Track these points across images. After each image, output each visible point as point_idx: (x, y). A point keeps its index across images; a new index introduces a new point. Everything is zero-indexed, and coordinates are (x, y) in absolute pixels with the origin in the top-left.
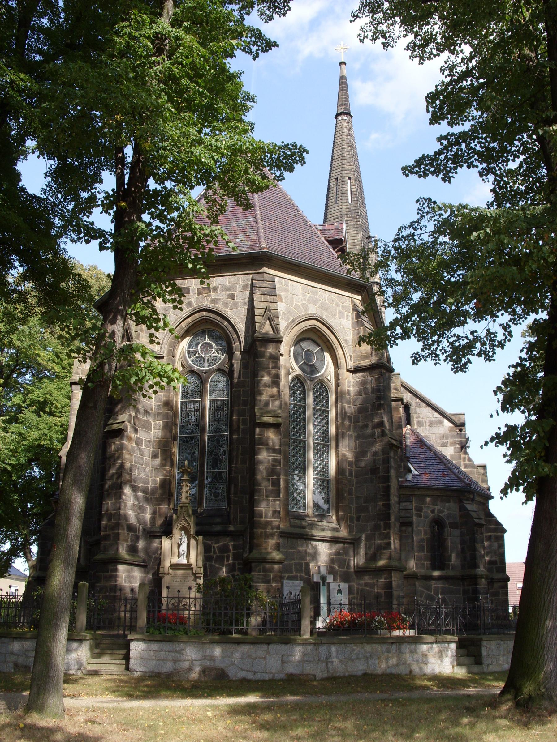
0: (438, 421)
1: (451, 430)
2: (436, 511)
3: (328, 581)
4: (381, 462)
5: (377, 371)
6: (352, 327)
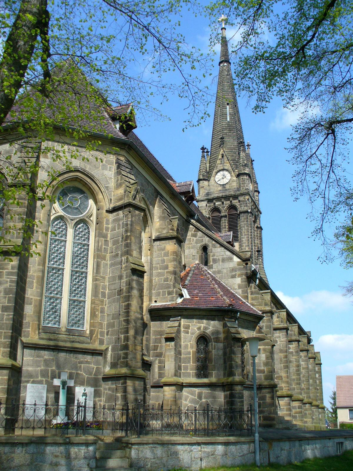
0: (229, 257)
1: (239, 264)
2: (202, 328)
3: (68, 385)
4: (125, 285)
5: (127, 209)
6: (114, 177)
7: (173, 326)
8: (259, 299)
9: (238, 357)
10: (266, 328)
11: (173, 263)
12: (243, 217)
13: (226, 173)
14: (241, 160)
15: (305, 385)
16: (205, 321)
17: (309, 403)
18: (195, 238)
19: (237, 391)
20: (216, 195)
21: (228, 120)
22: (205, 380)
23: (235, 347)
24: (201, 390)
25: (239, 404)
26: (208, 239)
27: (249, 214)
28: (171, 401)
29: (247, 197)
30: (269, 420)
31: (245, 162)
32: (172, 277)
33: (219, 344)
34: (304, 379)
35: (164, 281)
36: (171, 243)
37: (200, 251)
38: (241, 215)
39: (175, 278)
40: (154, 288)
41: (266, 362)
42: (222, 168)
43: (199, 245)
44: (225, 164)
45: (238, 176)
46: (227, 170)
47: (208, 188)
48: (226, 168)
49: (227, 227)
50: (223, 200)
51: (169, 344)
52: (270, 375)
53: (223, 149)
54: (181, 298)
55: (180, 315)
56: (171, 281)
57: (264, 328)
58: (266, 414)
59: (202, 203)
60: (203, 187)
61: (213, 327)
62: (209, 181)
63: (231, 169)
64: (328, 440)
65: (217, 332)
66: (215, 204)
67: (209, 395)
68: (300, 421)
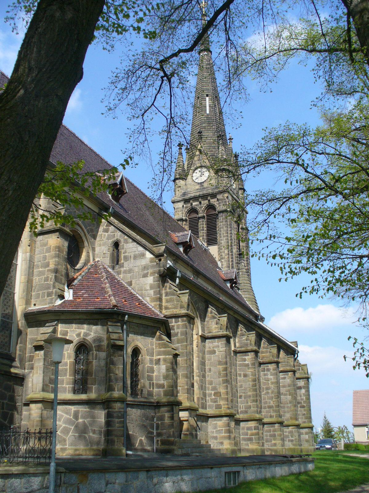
1: (151, 261)
2: (82, 335)
7: (46, 332)
8: (174, 300)
9: (118, 368)
10: (181, 335)
11: (54, 260)
12: (221, 217)
14: (220, 154)
15: (273, 402)
16: (85, 326)
17: (278, 423)
18: (106, 234)
19: (115, 409)
20: (193, 195)
21: (208, 112)
22: (83, 397)
23: (115, 357)
24: (77, 408)
25: (117, 425)
26: (120, 233)
28: (37, 421)
30: (168, 445)
31: (224, 157)
32: (52, 276)
33: (101, 353)
34: (273, 395)
35: (45, 281)
36: (53, 237)
37: (111, 248)
39: (56, 277)
40: (34, 290)
41: (166, 374)
42: (199, 165)
43: (110, 241)
45: (217, 172)
46: (205, 167)
47: (185, 187)
49: (205, 229)
50: (200, 200)
51: (39, 354)
52: (173, 390)
53: (201, 144)
54: (61, 300)
55: (58, 320)
56: (51, 281)
57: (179, 334)
58: (164, 437)
59: (179, 204)
61: (95, 333)
62: (186, 180)
64: (209, 470)
65: (98, 340)
66: (192, 204)
67: (87, 414)
68: (256, 444)
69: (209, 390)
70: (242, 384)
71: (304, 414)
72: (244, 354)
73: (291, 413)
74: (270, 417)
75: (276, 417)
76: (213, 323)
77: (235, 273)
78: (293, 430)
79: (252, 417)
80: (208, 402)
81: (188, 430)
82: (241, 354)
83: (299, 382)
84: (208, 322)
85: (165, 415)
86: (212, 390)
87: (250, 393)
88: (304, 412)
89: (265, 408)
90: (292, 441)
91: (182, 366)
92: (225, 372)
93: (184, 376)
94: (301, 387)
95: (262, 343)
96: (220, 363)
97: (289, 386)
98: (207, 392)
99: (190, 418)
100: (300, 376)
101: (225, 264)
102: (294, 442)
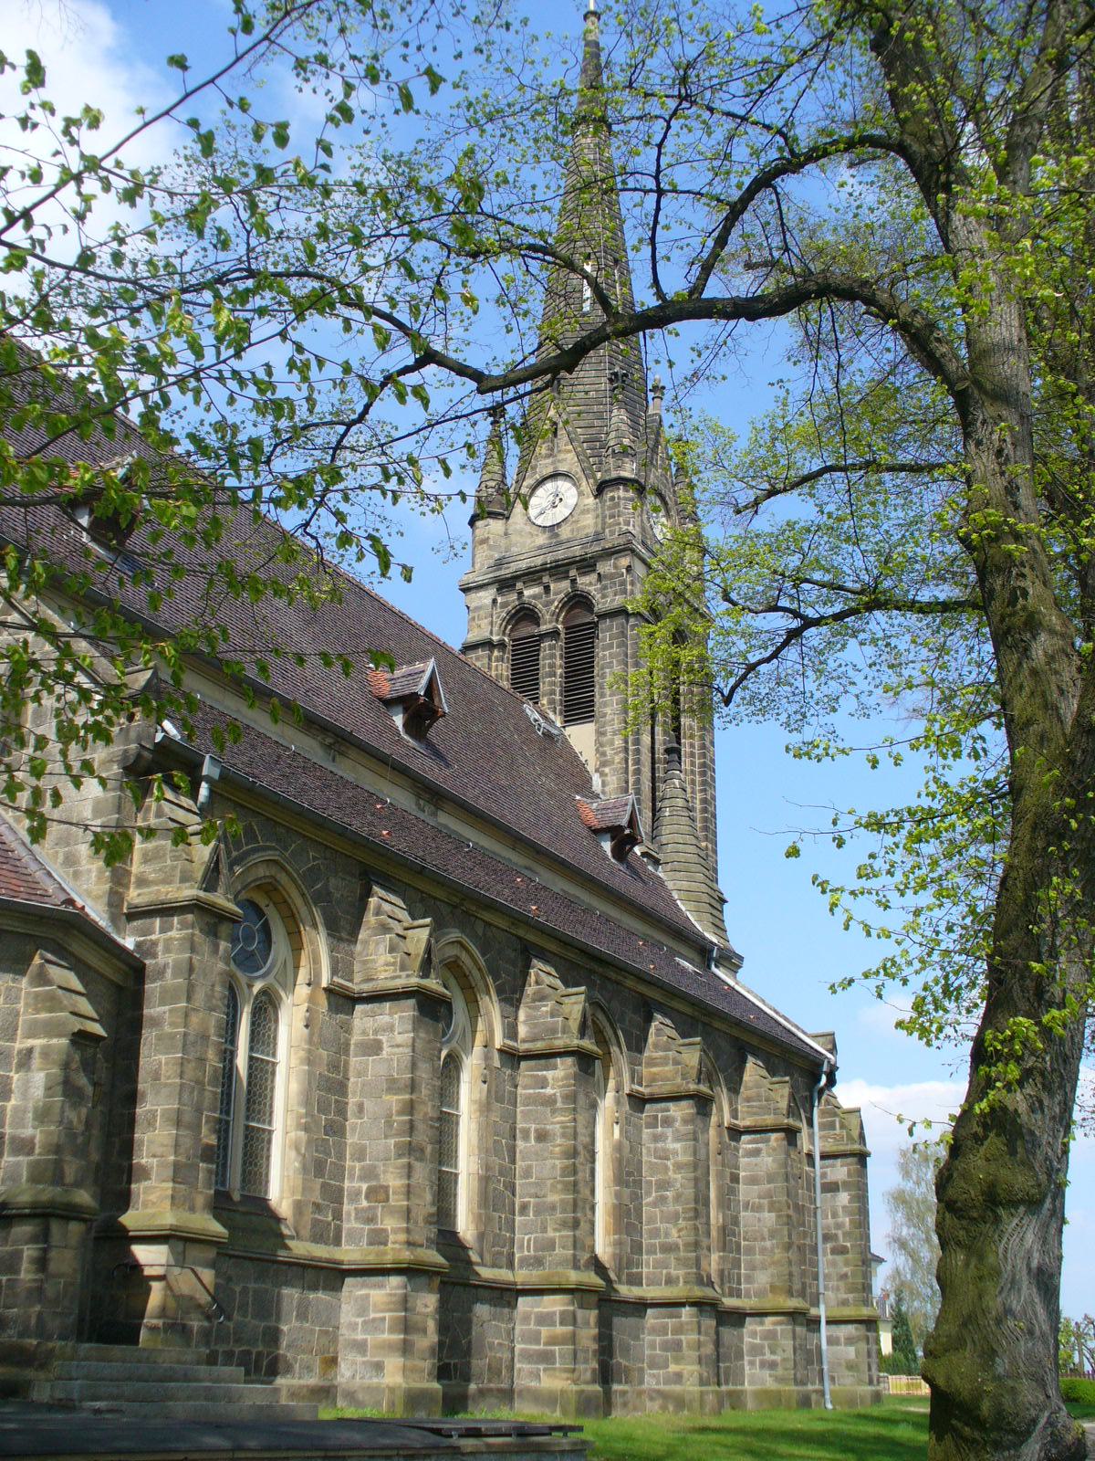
8: (164, 855)
10: (175, 976)
12: (607, 634)
13: (563, 486)
14: (613, 435)
15: (680, 1231)
17: (693, 1304)
20: (523, 565)
27: (632, 621)
29: (625, 561)
34: (680, 1208)
38: (603, 625)
41: (45, 1104)
42: (550, 470)
44: (561, 456)
45: (601, 489)
46: (566, 476)
47: (503, 542)
48: (563, 468)
49: (559, 671)
50: (546, 579)
59: (482, 594)
60: (484, 541)
62: (508, 518)
63: (579, 469)
66: (520, 594)
68: (565, 1375)
69: (352, 1177)
70: (530, 1167)
71: (844, 1277)
72: (543, 1062)
73: (771, 1270)
74: (666, 1283)
75: (686, 1282)
76: (382, 949)
77: (629, 808)
78: (779, 1328)
79: (556, 1281)
80: (349, 1221)
81: (163, 1312)
82: (532, 1063)
83: (833, 1166)
84: (366, 943)
85: (22, 1251)
86: (362, 1178)
87: (553, 1198)
88: (845, 1269)
89: (651, 1251)
90: (773, 1365)
91: (166, 1085)
92: (407, 1118)
93: (168, 1120)
94: (836, 1184)
95: (652, 1030)
96: (392, 1086)
97: (771, 1179)
98: (347, 1184)
99: (177, 1270)
100: (834, 1148)
101: (613, 781)
102: (780, 1372)
